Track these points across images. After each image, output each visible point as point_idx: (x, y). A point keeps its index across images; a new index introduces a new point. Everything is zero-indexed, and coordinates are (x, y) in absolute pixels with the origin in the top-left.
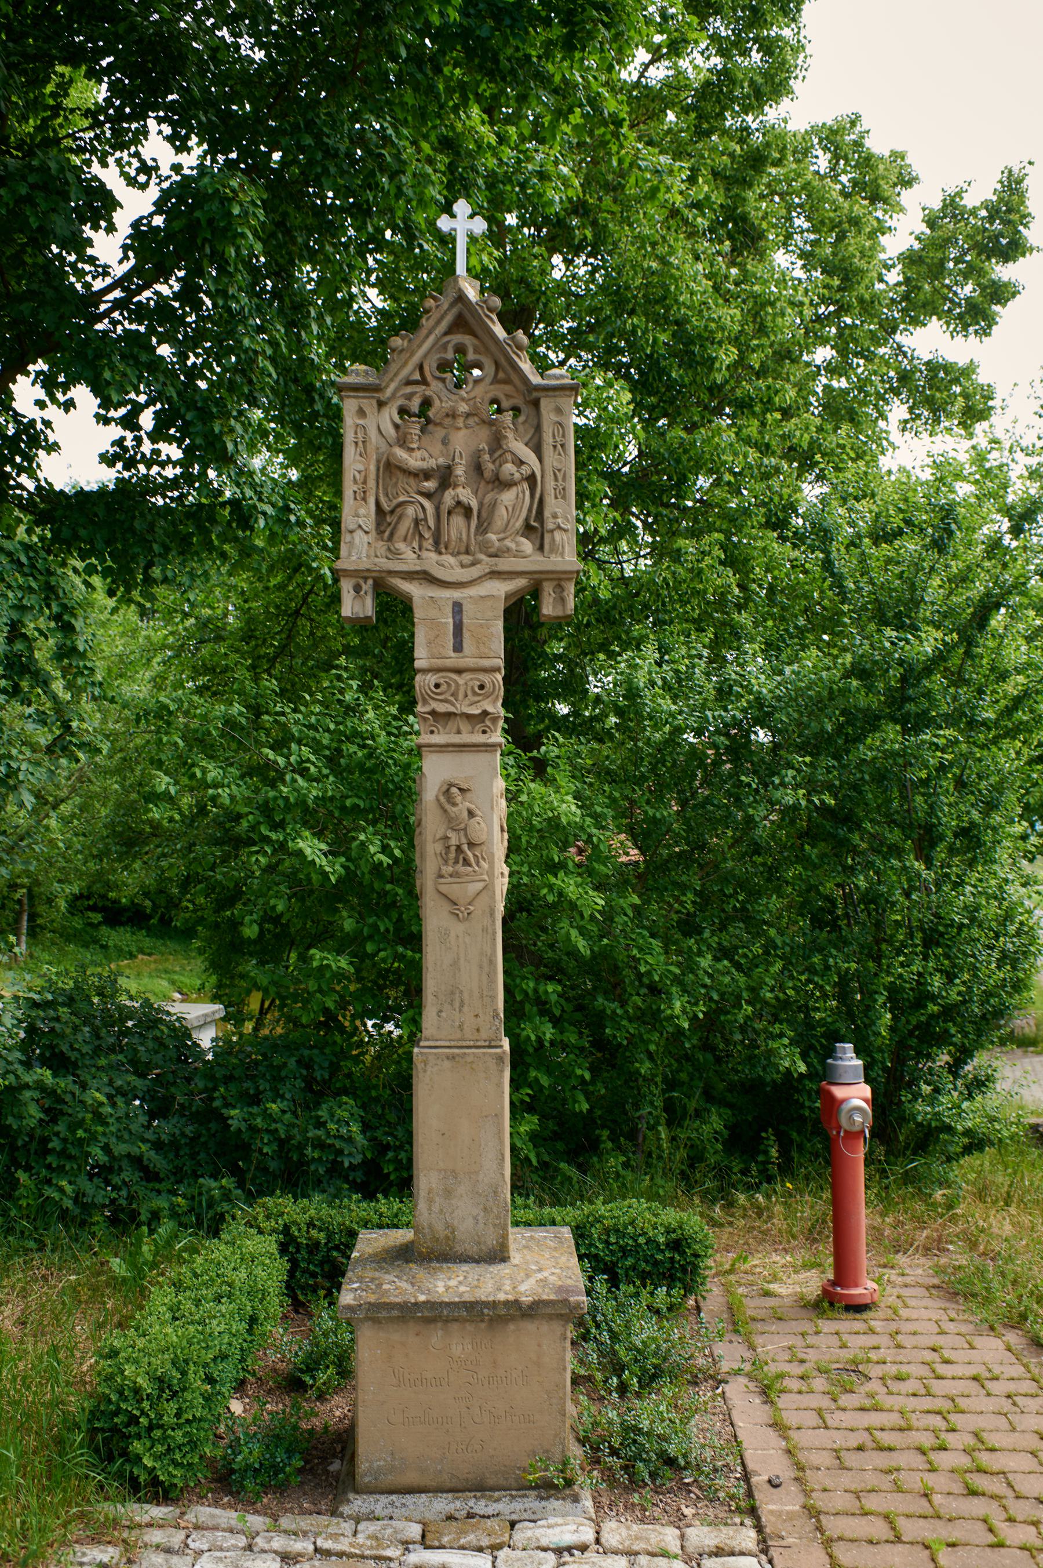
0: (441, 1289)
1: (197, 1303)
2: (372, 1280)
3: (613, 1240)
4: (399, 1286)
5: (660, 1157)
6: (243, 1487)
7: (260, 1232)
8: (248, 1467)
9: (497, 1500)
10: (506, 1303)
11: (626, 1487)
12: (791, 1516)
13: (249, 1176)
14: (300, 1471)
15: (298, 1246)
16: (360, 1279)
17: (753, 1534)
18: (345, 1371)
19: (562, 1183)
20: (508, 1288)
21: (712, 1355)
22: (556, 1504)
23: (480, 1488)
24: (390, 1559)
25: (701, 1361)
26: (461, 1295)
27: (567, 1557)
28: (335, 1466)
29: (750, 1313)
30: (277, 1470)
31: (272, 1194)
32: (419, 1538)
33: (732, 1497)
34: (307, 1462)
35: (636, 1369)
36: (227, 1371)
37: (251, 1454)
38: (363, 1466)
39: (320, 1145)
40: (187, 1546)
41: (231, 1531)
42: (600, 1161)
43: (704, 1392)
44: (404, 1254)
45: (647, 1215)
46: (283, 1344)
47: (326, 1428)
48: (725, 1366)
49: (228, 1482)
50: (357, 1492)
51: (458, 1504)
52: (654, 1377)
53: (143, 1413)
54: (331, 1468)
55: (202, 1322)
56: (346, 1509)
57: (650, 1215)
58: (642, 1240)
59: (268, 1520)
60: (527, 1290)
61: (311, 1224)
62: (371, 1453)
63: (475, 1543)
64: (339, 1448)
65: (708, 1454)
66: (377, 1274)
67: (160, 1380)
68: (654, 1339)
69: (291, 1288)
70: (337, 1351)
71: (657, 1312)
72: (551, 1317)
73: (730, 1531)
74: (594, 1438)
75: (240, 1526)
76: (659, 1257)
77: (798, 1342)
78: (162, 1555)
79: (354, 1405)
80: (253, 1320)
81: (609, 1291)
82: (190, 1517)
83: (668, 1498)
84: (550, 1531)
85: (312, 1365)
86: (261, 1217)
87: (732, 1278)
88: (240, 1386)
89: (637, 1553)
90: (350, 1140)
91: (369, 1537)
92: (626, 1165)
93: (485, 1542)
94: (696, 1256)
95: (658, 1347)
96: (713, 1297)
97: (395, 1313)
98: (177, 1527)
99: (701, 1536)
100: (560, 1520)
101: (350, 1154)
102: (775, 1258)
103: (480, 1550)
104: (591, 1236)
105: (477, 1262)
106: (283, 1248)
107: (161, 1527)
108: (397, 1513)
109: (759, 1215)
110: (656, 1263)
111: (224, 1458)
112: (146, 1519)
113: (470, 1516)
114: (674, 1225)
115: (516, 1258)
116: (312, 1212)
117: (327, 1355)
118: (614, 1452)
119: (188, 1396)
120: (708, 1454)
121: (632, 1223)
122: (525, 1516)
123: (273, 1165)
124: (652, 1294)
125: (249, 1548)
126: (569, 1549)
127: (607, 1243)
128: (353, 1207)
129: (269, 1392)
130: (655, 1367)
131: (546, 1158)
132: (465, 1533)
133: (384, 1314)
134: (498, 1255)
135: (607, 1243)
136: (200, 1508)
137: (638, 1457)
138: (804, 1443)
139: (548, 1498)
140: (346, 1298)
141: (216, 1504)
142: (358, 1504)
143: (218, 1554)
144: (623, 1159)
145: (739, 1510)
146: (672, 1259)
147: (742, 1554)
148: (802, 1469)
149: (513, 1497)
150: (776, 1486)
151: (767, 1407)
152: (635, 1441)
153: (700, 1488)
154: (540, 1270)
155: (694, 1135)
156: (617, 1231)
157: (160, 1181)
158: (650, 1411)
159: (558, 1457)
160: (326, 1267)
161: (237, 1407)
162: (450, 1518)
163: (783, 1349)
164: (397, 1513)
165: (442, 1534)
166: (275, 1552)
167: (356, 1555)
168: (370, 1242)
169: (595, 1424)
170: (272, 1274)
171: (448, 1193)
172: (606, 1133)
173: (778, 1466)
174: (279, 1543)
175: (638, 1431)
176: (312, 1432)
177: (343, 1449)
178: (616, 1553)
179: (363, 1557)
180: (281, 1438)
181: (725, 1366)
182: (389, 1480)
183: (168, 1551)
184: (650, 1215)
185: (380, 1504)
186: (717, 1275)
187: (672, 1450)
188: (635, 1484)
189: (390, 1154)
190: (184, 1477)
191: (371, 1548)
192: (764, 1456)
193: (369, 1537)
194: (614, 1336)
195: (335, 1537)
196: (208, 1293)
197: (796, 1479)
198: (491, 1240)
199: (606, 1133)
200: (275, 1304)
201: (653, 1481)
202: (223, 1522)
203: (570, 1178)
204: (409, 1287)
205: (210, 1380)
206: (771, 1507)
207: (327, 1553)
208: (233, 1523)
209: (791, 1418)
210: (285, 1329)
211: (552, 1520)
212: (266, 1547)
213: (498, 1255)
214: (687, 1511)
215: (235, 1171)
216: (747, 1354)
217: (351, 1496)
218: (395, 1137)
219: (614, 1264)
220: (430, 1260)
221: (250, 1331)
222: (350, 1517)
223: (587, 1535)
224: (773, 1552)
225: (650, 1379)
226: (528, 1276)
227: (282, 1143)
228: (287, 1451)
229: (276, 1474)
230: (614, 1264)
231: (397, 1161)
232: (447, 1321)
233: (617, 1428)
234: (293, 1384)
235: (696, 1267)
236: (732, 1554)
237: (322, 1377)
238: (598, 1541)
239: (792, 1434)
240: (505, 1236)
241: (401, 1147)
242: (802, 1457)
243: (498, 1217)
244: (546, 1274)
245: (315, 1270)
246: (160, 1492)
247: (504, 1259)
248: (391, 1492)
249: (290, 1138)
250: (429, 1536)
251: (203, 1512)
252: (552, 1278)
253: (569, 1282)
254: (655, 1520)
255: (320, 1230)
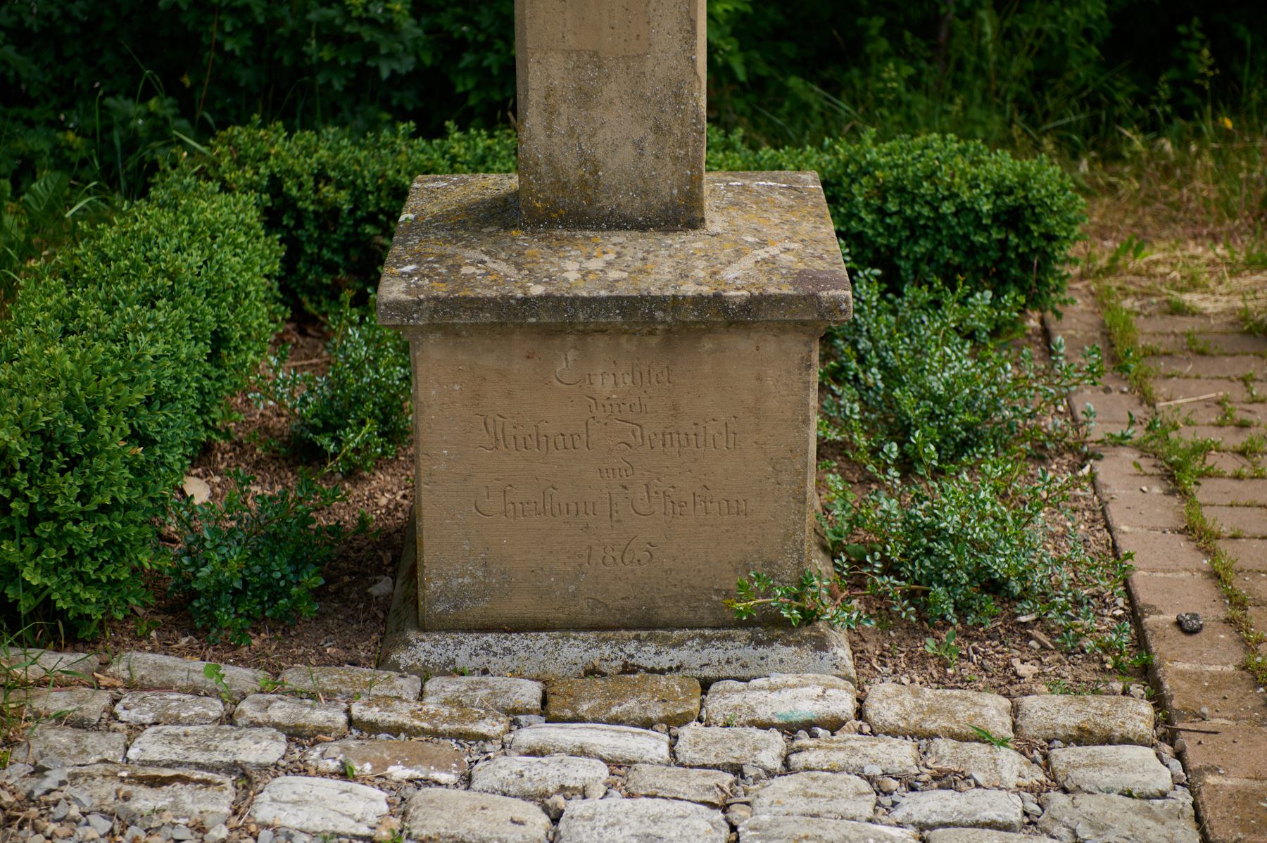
0: (573, 276)
1: (111, 306)
2: (441, 258)
3: (892, 206)
4: (489, 270)
5: (978, 71)
6: (214, 621)
7: (226, 188)
8: (221, 587)
9: (678, 644)
10: (698, 300)
11: (910, 628)
12: (1218, 682)
13: (201, 94)
14: (317, 594)
15: (300, 216)
16: (418, 258)
17: (1147, 709)
18: (395, 430)
19: (791, 115)
20: (701, 274)
21: (1071, 411)
22: (786, 652)
23: (648, 624)
24: (486, 738)
25: (1050, 423)
26: (612, 285)
27: (804, 739)
28: (382, 587)
29: (1142, 342)
30: (274, 592)
31: (244, 121)
32: (536, 704)
33: (1107, 648)
34: (329, 580)
35: (932, 429)
36: (176, 425)
37: (226, 563)
38: (431, 585)
39: (332, 36)
40: (114, 716)
41: (195, 691)
42: (866, 74)
43: (1058, 473)
44: (501, 216)
45: (961, 163)
46: (277, 384)
47: (363, 522)
48: (1097, 431)
49: (183, 613)
50: (423, 629)
51: (606, 650)
52: (964, 446)
53: (16, 493)
54: (375, 591)
55: (119, 338)
56: (403, 657)
57: (966, 164)
58: (947, 208)
59: (261, 674)
60: (738, 277)
61: (321, 176)
62: (444, 565)
63: (637, 712)
64: (387, 557)
65: (1065, 574)
66: (449, 249)
67: (45, 436)
68: (968, 380)
69: (289, 287)
70: (380, 397)
71: (971, 335)
72: (782, 328)
73: (1106, 704)
74: (852, 545)
75: (211, 683)
76: (980, 239)
77: (1237, 392)
78: (69, 732)
79: (413, 489)
80: (219, 340)
81: (883, 295)
82: (119, 668)
83: (989, 647)
84: (774, 696)
85: (332, 421)
86: (225, 162)
87: (1113, 283)
88: (202, 457)
89: (932, 736)
90: (389, 27)
91: (446, 703)
92: (913, 83)
93: (656, 712)
94: (1050, 237)
95: (975, 394)
96: (1075, 319)
97: (486, 317)
98: (96, 686)
99: (1049, 709)
100: (792, 679)
101: (391, 55)
102: (1193, 248)
103: (648, 724)
104: (850, 200)
105: (642, 228)
106: (271, 219)
107: (64, 685)
108: (495, 663)
109: (1167, 172)
110: (973, 251)
111: (177, 572)
112: (35, 672)
113: (628, 669)
114: (1011, 179)
115: (716, 222)
116: (323, 152)
117: (359, 402)
118: (890, 569)
119: (101, 464)
120: (1065, 574)
121: (931, 176)
122: (728, 670)
123: (245, 76)
124: (963, 302)
125: (229, 719)
126: (809, 726)
127: (882, 212)
128: (400, 143)
129: (257, 465)
130: (968, 427)
131: (763, 70)
132: (621, 697)
133: (465, 319)
134: (682, 215)
135: (882, 212)
136: (136, 655)
137: (934, 577)
138: (1245, 561)
139: (770, 643)
140: (392, 289)
141: (166, 648)
142: (424, 648)
143: (172, 729)
144: (908, 71)
145: (1119, 669)
146: (1003, 244)
147: (1126, 741)
148: (1242, 605)
149: (706, 640)
150: (1192, 632)
151: (1175, 501)
152: (929, 551)
153: (1049, 632)
154: (763, 243)
155: (1048, 26)
156: (901, 190)
157: (31, 103)
158: (960, 502)
159: (790, 573)
160: (354, 254)
161: (198, 490)
162: (592, 672)
163: (1207, 404)
164: (495, 663)
165: (578, 699)
166: (277, 726)
167: (423, 732)
168: (433, 194)
169: (855, 522)
170: (253, 261)
171: (585, 97)
172: (877, 23)
173: (1199, 599)
174: (281, 711)
175: (937, 533)
176: (336, 530)
177: (396, 559)
178: (894, 733)
179: (436, 734)
180: (277, 538)
181: (1097, 431)
182: (479, 609)
183: (80, 724)
184: (966, 164)
185: (465, 649)
186: (1082, 277)
187: (999, 565)
188: (928, 621)
189: (468, 59)
190: (103, 604)
191: (451, 719)
192: (1169, 581)
193: (446, 703)
194: (892, 375)
195: (385, 702)
196: (134, 289)
197: (1228, 621)
198: (668, 187)
199: (877, 23)
200: (262, 314)
201: (962, 618)
202: (180, 678)
203: (806, 107)
204: (511, 271)
205: (139, 437)
206: (1180, 666)
207: (372, 728)
208: (198, 678)
209: (1220, 520)
210: (282, 359)
211: (776, 679)
212: (260, 717)
213: (682, 215)
214: (1026, 670)
215: (172, 88)
216: (1139, 412)
217: (412, 635)
218: (476, 26)
219: (893, 251)
220: (552, 224)
221: (214, 357)
222: (411, 670)
223: (843, 703)
224: (1183, 739)
225: (959, 448)
226: (739, 253)
227: (260, 33)
228: (293, 561)
229: (274, 599)
230: (893, 251)
231: (481, 71)
232: (584, 332)
233: (896, 527)
234: (301, 452)
235: (1047, 258)
236: (1108, 740)
237: (353, 439)
238: (860, 714)
239: (1222, 546)
240: (696, 182)
241: (487, 45)
242: (1241, 585)
243: (682, 144)
244: (774, 250)
245: (330, 255)
246: (61, 629)
247: (694, 222)
248: (485, 629)
249: (275, 23)
250: (554, 702)
251: (144, 662)
252: (786, 258)
253: (819, 265)
254: (965, 683)
255: (340, 186)
